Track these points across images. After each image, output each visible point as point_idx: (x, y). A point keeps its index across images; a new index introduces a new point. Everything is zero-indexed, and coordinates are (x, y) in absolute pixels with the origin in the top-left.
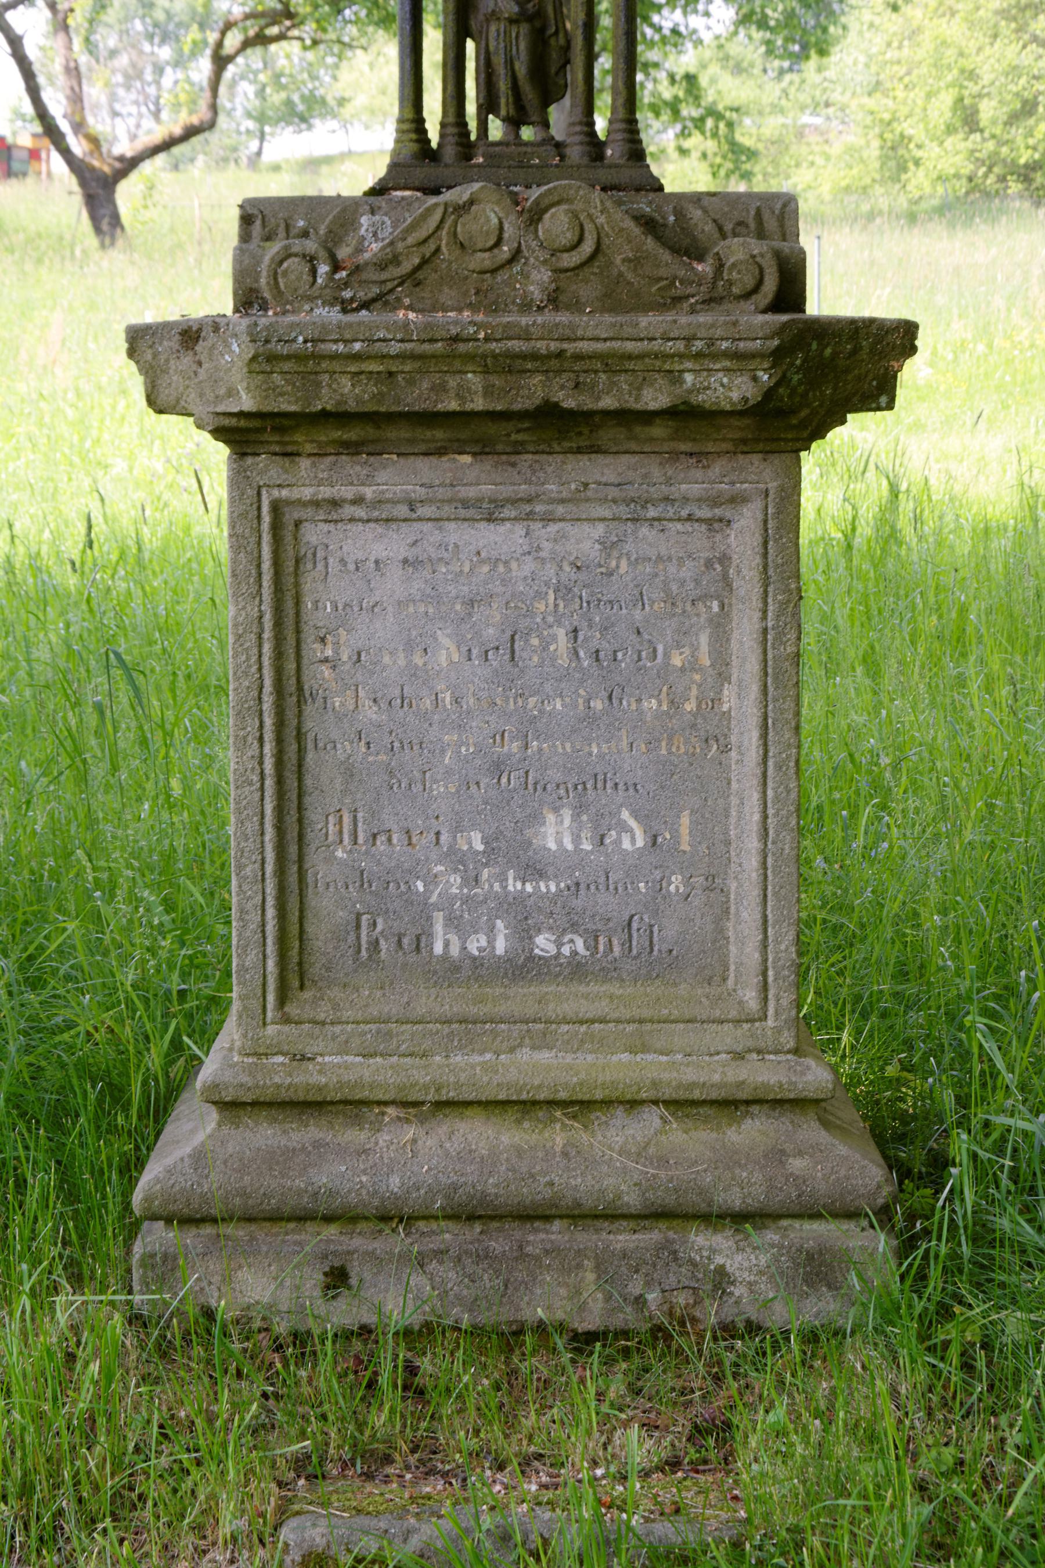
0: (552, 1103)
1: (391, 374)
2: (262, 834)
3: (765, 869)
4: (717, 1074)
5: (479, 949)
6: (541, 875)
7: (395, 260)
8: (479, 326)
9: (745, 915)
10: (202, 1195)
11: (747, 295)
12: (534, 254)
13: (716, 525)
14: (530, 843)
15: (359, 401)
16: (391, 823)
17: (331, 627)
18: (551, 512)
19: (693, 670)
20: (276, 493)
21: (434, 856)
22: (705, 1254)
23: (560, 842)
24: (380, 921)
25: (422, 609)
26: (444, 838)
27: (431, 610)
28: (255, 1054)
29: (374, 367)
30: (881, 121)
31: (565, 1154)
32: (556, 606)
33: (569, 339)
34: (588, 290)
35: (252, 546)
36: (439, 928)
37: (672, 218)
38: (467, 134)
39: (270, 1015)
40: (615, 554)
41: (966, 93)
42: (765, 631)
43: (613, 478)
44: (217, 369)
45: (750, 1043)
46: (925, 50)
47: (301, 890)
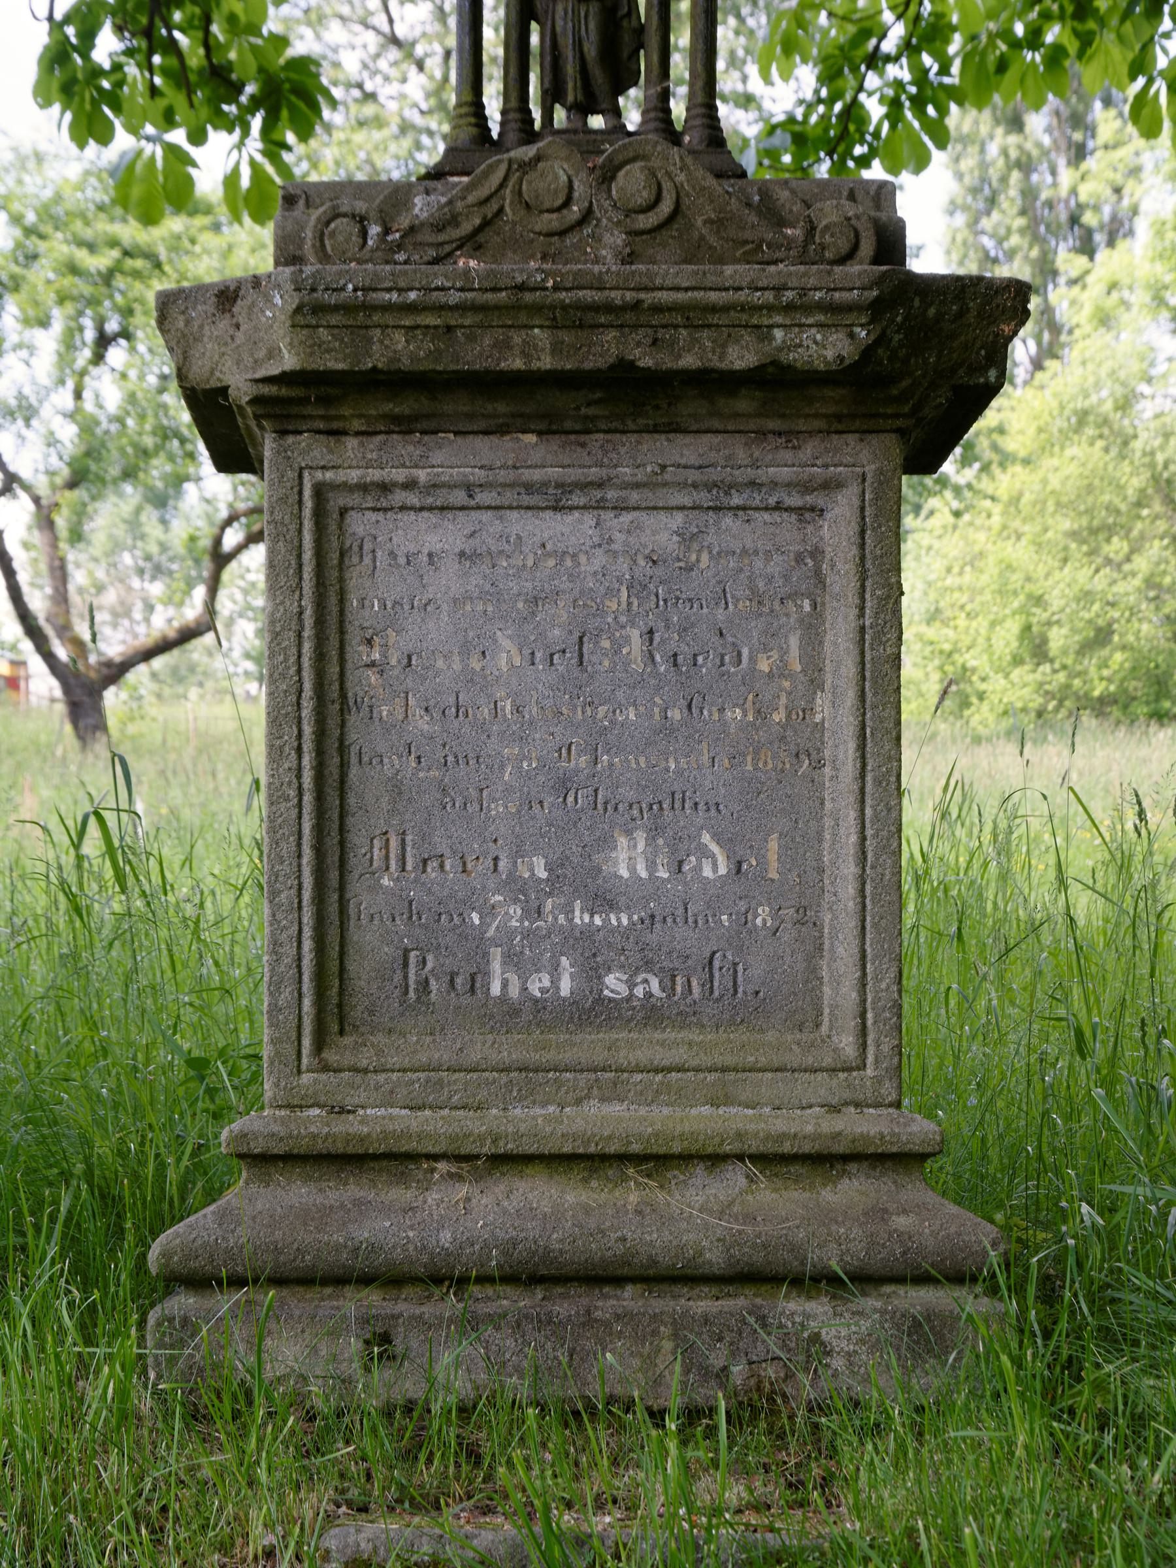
0: (623, 1158)
1: (449, 329)
2: (300, 856)
3: (864, 897)
4: (809, 1125)
5: (541, 990)
6: (612, 906)
7: (454, 220)
8: (547, 274)
9: (840, 950)
10: (227, 1251)
12: (606, 215)
13: (807, 515)
14: (600, 870)
15: (414, 358)
16: (443, 848)
17: (379, 627)
18: (624, 500)
19: (782, 676)
20: (319, 475)
21: (491, 885)
22: (798, 1319)
23: (632, 869)
24: (430, 958)
25: (480, 608)
26: (502, 864)
27: (490, 609)
28: (289, 1106)
29: (431, 320)
30: (941, 652)
31: (639, 1212)
32: (629, 604)
33: (646, 289)
35: (292, 533)
36: (496, 966)
37: (757, 198)
38: (532, 121)
39: (305, 1061)
40: (695, 546)
41: (1034, 620)
42: (862, 629)
43: (693, 460)
44: (256, 329)
45: (847, 1095)
46: (991, 569)
47: (342, 923)
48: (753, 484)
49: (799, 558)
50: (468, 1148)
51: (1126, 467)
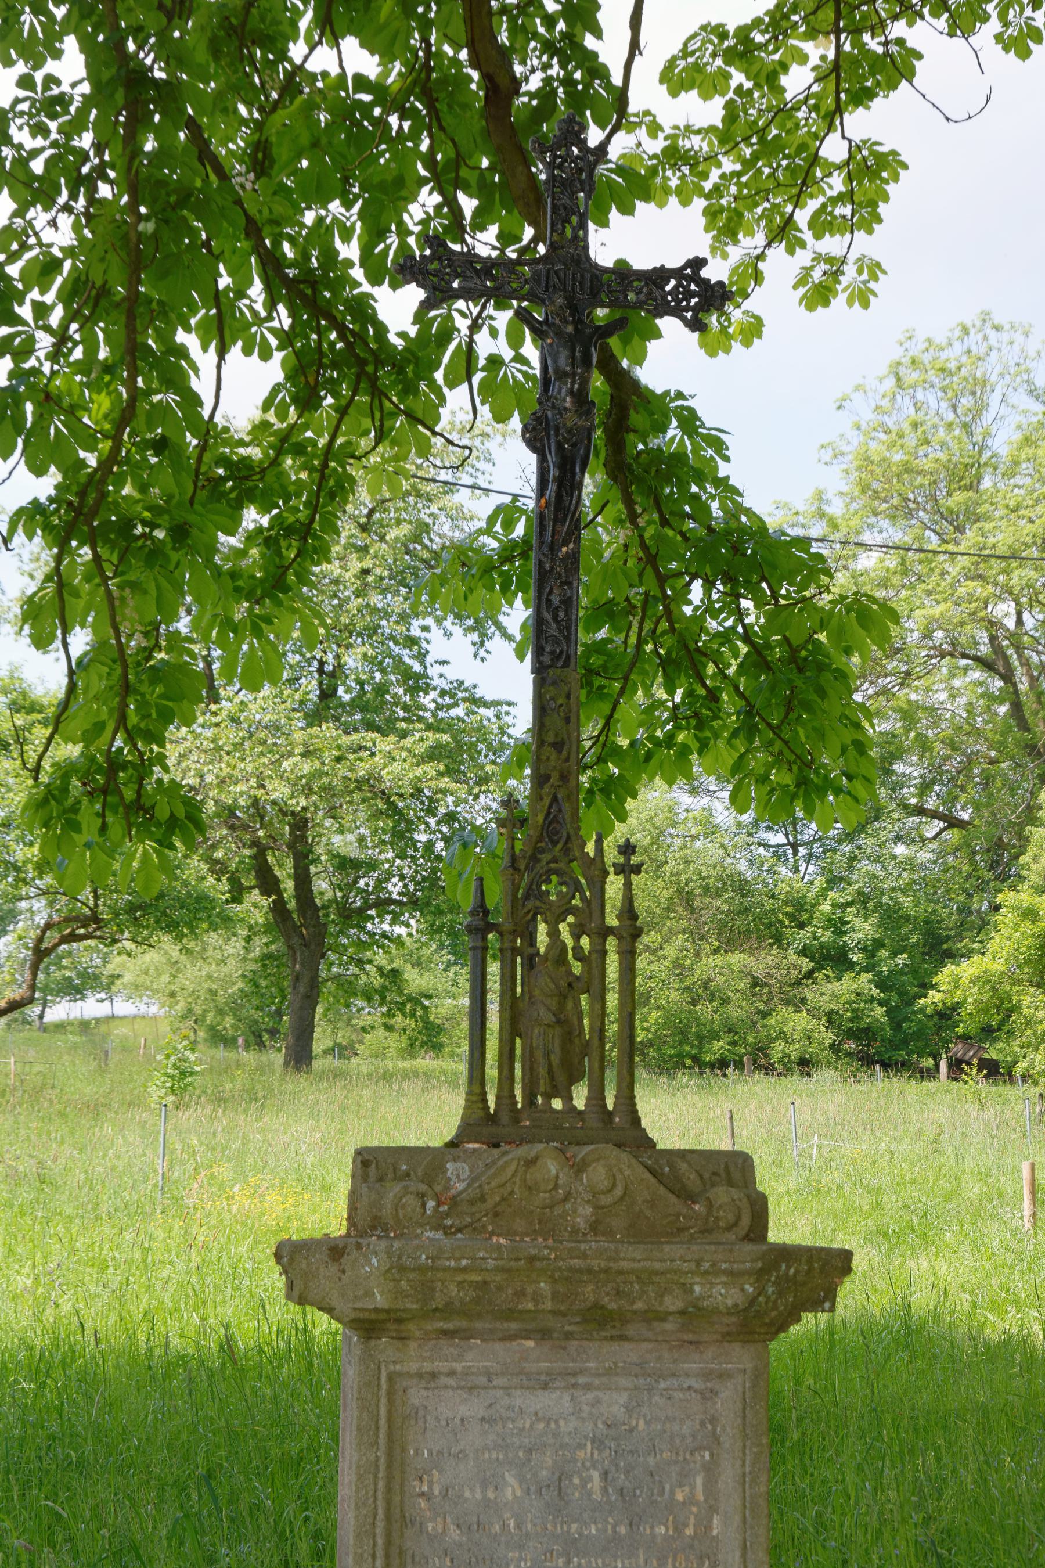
1: (485, 1282)
11: (729, 1228)
49: (702, 1424)
51: (660, 883)
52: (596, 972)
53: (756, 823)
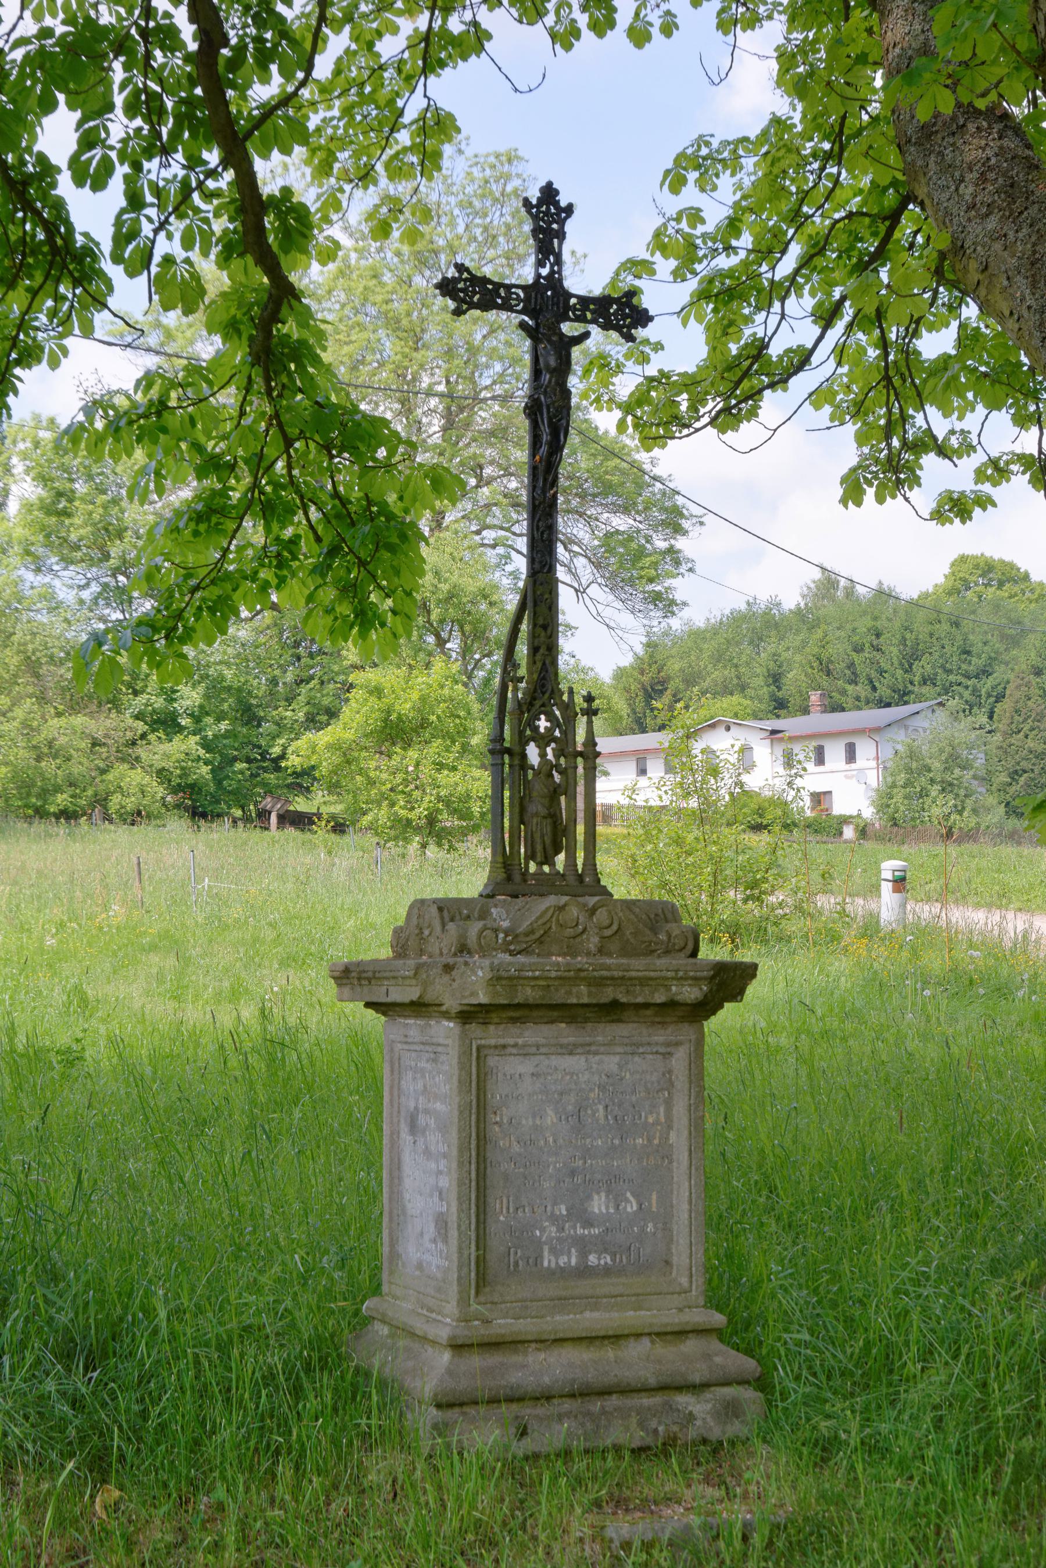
0: (604, 1337)
4: (674, 1319)
7: (532, 932)
9: (681, 1241)
11: (681, 950)
26: (549, 1208)
34: (614, 946)
36: (546, 1253)
48: (649, 1044)
50: (545, 1337)
52: (571, 781)
53: (95, 600)
